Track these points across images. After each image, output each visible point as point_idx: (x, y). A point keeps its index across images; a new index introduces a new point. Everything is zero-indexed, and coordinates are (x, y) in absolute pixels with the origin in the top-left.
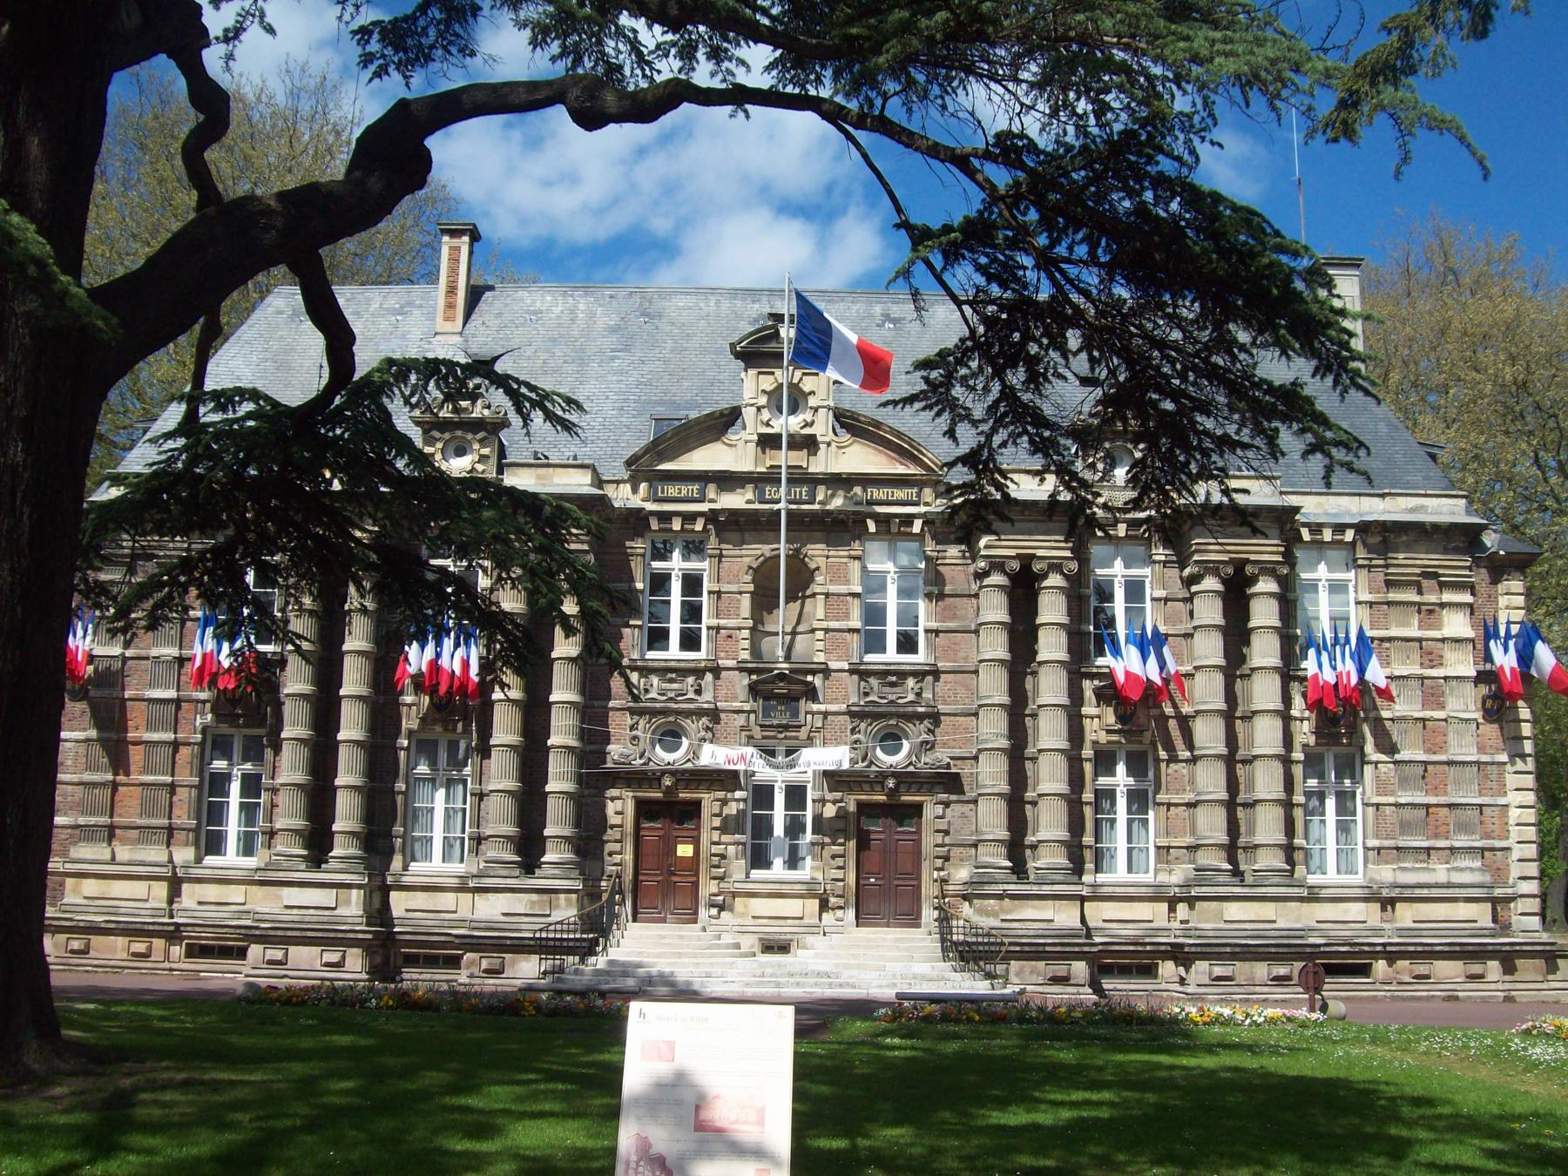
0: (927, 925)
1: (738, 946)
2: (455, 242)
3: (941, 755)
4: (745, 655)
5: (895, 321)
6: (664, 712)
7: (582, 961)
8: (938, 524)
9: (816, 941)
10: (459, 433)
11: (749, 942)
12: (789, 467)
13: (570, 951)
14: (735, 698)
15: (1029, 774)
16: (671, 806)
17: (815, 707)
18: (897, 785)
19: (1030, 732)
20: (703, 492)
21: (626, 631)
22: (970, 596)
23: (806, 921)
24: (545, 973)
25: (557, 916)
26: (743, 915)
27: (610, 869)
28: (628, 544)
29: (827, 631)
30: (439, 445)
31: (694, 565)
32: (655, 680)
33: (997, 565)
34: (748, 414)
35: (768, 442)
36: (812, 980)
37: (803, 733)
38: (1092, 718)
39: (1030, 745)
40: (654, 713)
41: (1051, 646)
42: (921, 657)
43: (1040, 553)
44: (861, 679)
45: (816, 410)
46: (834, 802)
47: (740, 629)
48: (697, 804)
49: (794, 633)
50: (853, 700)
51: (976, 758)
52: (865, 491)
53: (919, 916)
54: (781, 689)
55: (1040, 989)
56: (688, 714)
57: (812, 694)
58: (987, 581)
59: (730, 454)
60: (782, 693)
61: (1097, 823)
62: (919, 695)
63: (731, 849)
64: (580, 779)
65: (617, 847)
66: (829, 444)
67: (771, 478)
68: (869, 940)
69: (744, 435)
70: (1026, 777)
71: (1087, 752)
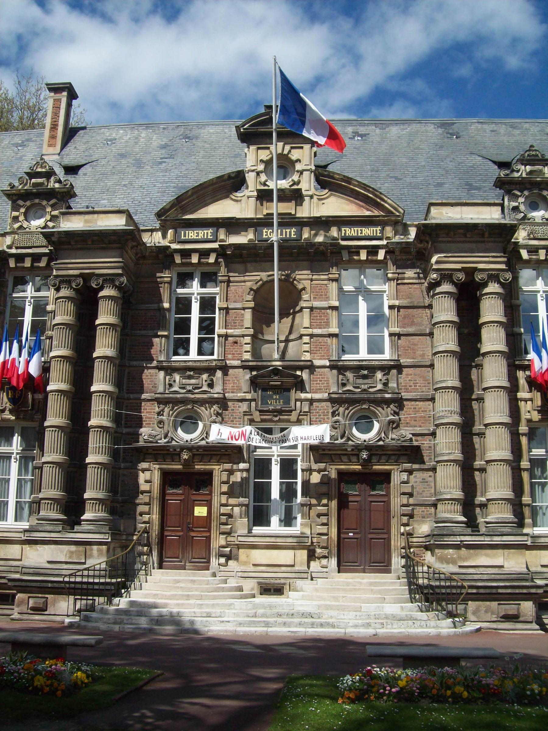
0: (396, 570)
1: (240, 589)
2: (58, 96)
3: (406, 432)
4: (247, 356)
5: (362, 136)
6: (184, 401)
7: (110, 602)
8: (397, 253)
9: (305, 585)
10: (37, 201)
11: (250, 586)
12: (279, 214)
13: (100, 593)
14: (239, 390)
15: (477, 446)
16: (189, 476)
17: (303, 396)
18: (370, 457)
19: (476, 413)
20: (216, 234)
21: (156, 340)
22: (425, 307)
23: (297, 568)
24: (80, 611)
25: (90, 563)
26: (245, 563)
27: (141, 526)
28: (158, 275)
29: (312, 336)
30: (23, 210)
31: (210, 290)
32: (177, 377)
33: (446, 276)
34: (250, 178)
35: (264, 196)
36: (296, 620)
37: (294, 417)
38: (526, 400)
39: (477, 423)
40: (175, 402)
41: (493, 340)
42: (387, 355)
43: (481, 266)
44: (340, 373)
45: (301, 173)
46: (319, 471)
47: (243, 336)
48: (209, 474)
49: (287, 341)
50: (334, 389)
51: (433, 434)
52: (340, 230)
53: (389, 564)
54: (276, 381)
55: (494, 625)
56: (203, 402)
57: (300, 385)
58: (438, 290)
59: (238, 207)
60: (276, 385)
61: (532, 485)
62: (386, 384)
63: (237, 510)
64: (115, 454)
65: (146, 508)
66: (311, 197)
67: (266, 222)
68: (348, 584)
69: (247, 193)
70: (474, 449)
71: (523, 428)
